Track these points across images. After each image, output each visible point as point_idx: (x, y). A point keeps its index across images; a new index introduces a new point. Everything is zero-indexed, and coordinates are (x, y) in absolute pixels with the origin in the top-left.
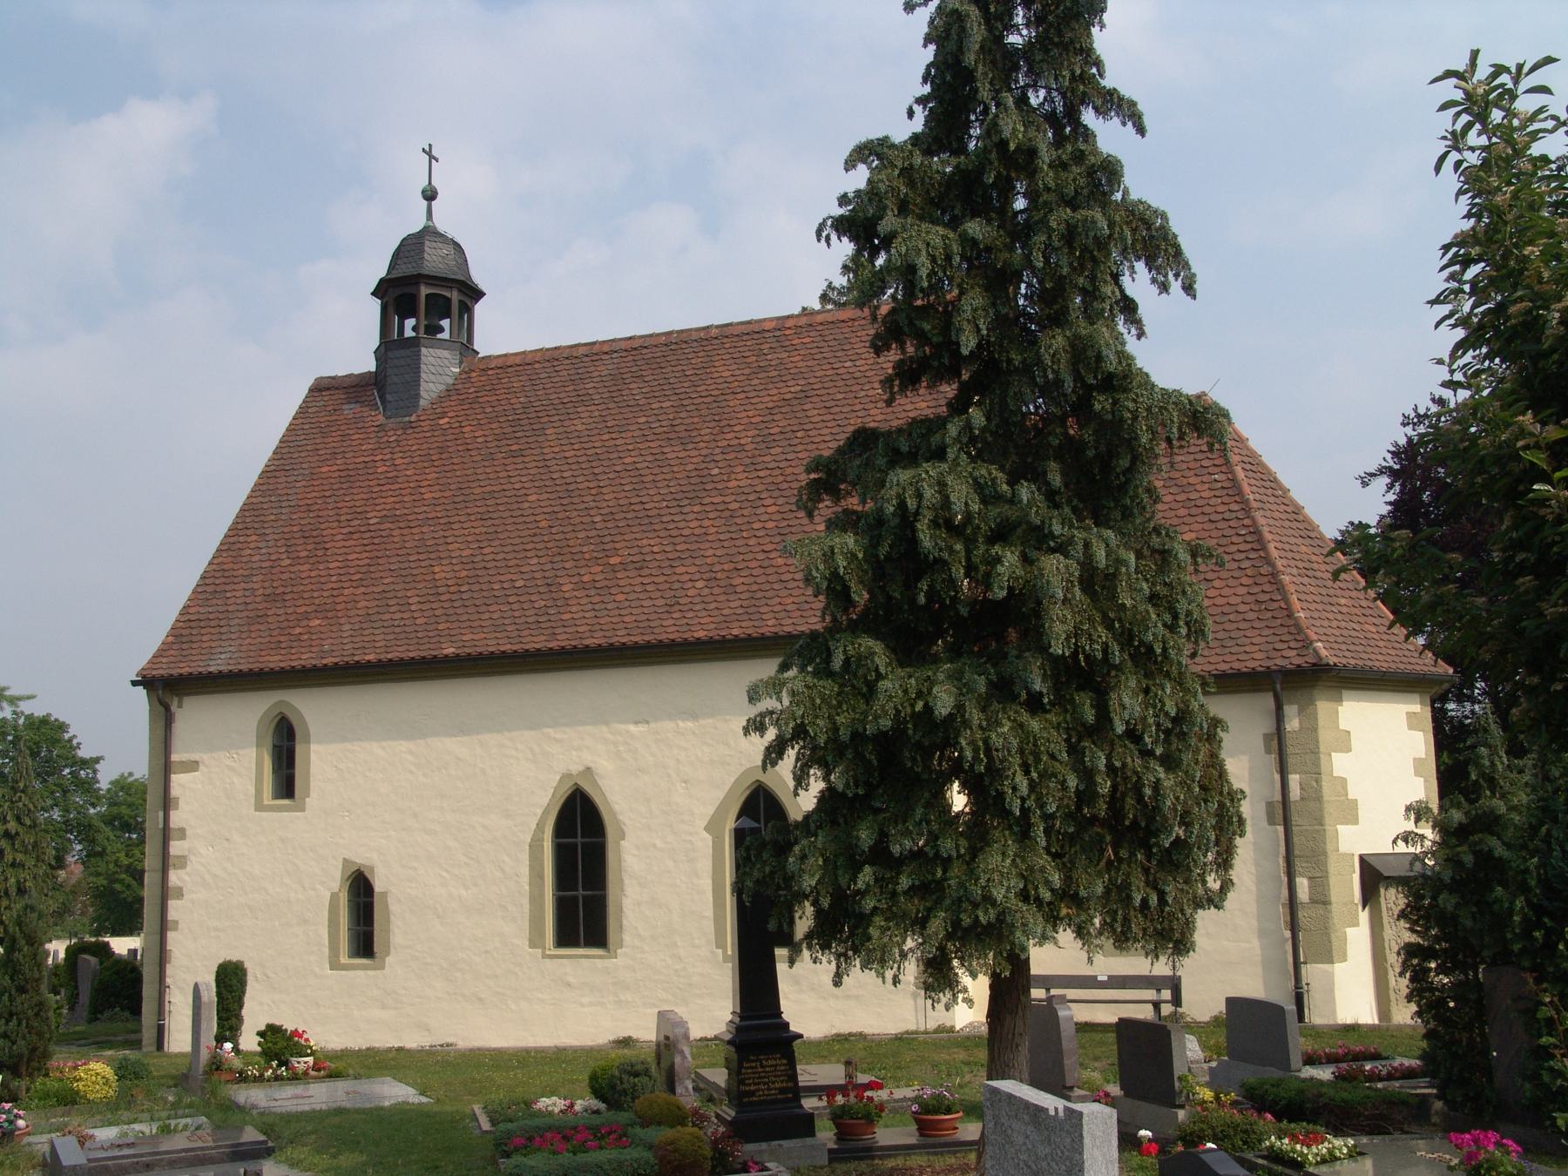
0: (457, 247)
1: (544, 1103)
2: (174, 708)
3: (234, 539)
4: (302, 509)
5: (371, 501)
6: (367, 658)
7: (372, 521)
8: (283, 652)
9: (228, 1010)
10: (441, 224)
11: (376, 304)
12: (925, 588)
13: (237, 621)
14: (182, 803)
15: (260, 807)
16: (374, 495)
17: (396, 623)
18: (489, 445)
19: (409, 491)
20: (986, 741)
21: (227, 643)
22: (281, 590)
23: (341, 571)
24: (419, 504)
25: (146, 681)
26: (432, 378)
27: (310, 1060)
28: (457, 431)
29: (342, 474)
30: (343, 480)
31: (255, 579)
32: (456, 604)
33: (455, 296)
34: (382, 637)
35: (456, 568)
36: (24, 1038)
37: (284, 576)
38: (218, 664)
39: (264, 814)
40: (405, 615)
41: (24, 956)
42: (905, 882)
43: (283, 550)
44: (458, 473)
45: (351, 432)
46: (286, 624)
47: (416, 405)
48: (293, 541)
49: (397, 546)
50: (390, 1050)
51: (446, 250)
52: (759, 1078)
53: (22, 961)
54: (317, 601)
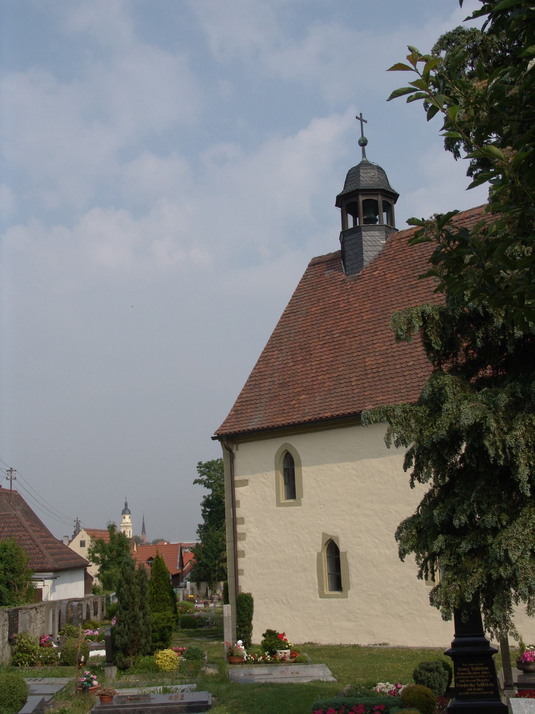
0: (380, 169)
1: (381, 686)
2: (234, 451)
3: (267, 354)
4: (301, 333)
5: (336, 324)
6: (326, 415)
7: (335, 336)
8: (285, 415)
9: (242, 621)
10: (371, 158)
11: (338, 211)
12: (481, 335)
13: (265, 400)
14: (241, 504)
15: (279, 504)
16: (338, 321)
17: (343, 393)
18: (399, 283)
19: (356, 316)
20: (503, 442)
21: (259, 413)
22: (288, 380)
23: (318, 366)
24: (361, 322)
25: (219, 437)
26: (370, 248)
27: (288, 651)
28: (382, 277)
29: (322, 311)
30: (322, 314)
31: (275, 375)
32: (376, 379)
33: (380, 199)
34: (335, 402)
35: (377, 358)
36: (127, 634)
37: (289, 372)
38: (253, 425)
39: (281, 508)
40: (349, 389)
41: (125, 590)
42: (465, 546)
43: (290, 357)
44: (382, 302)
45: (328, 286)
46: (288, 399)
47: (361, 266)
48: (295, 352)
49: (347, 348)
50: (349, 646)
51: (373, 173)
52: (469, 679)
53: (124, 592)
54: (304, 385)
